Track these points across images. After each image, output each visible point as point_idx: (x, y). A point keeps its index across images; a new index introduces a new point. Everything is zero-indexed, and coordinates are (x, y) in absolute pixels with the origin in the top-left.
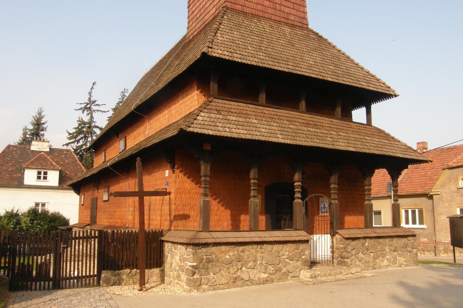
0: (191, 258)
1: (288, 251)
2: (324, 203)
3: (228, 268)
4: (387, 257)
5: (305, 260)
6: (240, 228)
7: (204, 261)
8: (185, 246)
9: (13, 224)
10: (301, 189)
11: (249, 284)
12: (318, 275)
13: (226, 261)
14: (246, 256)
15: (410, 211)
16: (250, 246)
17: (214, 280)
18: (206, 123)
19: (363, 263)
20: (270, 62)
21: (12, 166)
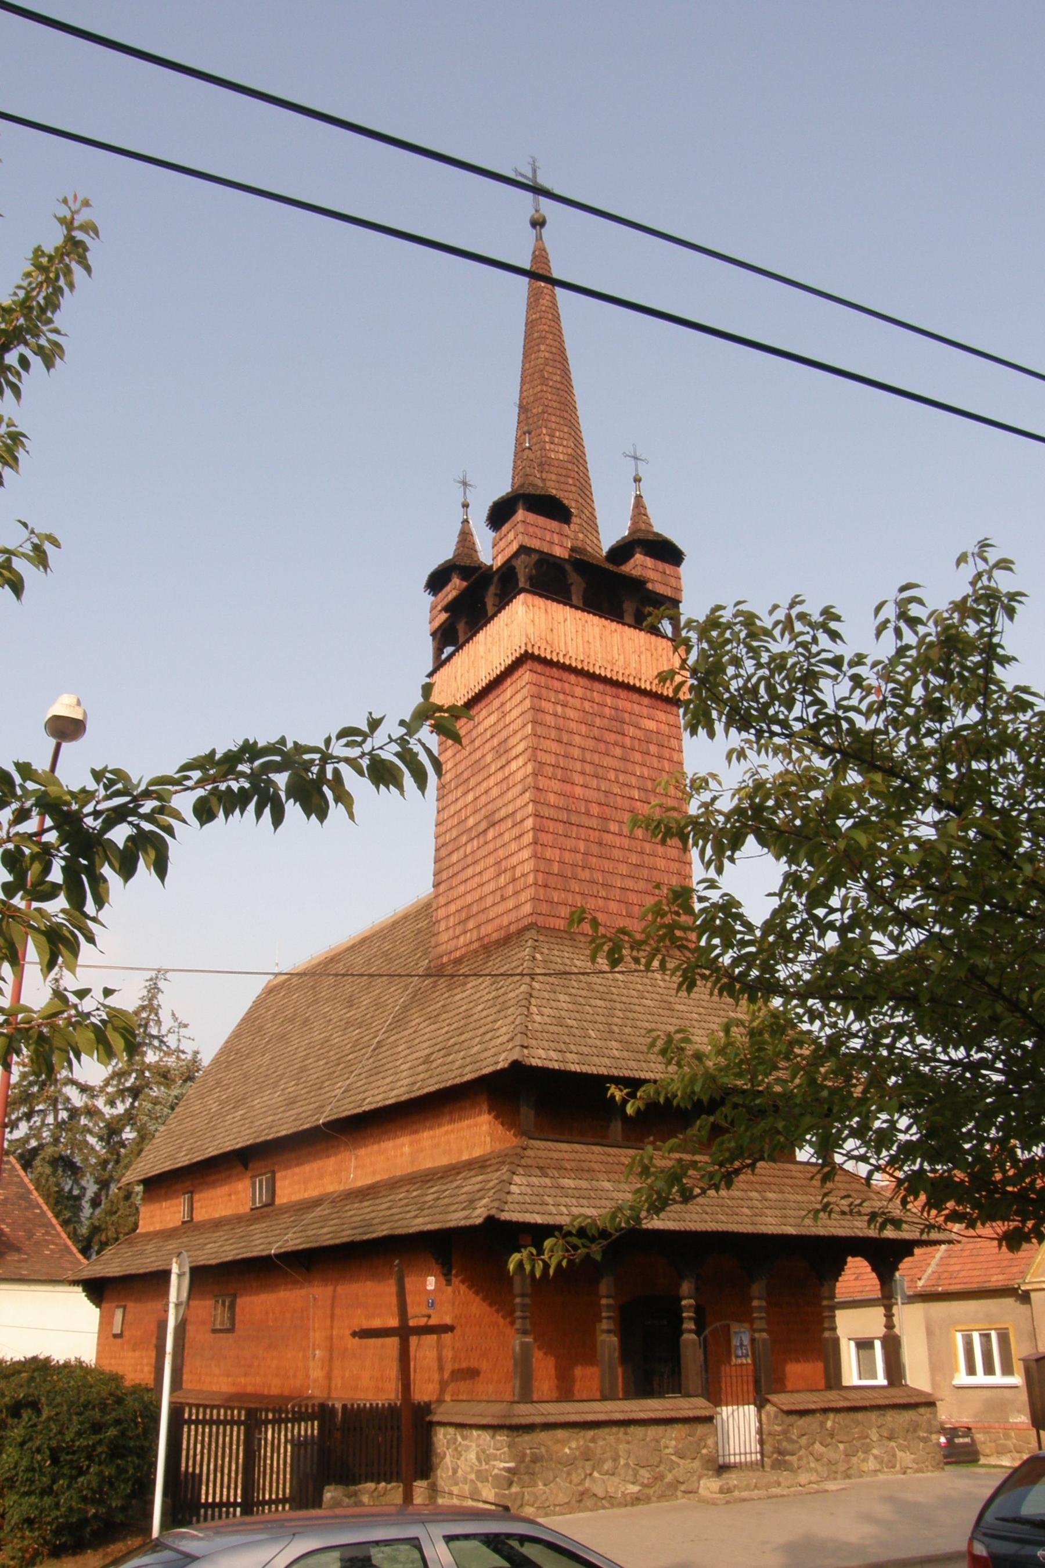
0: (504, 1453)
1: (676, 1439)
2: (741, 1337)
3: (569, 1474)
4: (875, 1451)
6: (573, 1395)
7: (528, 1459)
8: (491, 1432)
11: (607, 1505)
12: (735, 1486)
15: (976, 1337)
16: (607, 1430)
17: (544, 1497)
18: (527, 1199)
20: (633, 1064)
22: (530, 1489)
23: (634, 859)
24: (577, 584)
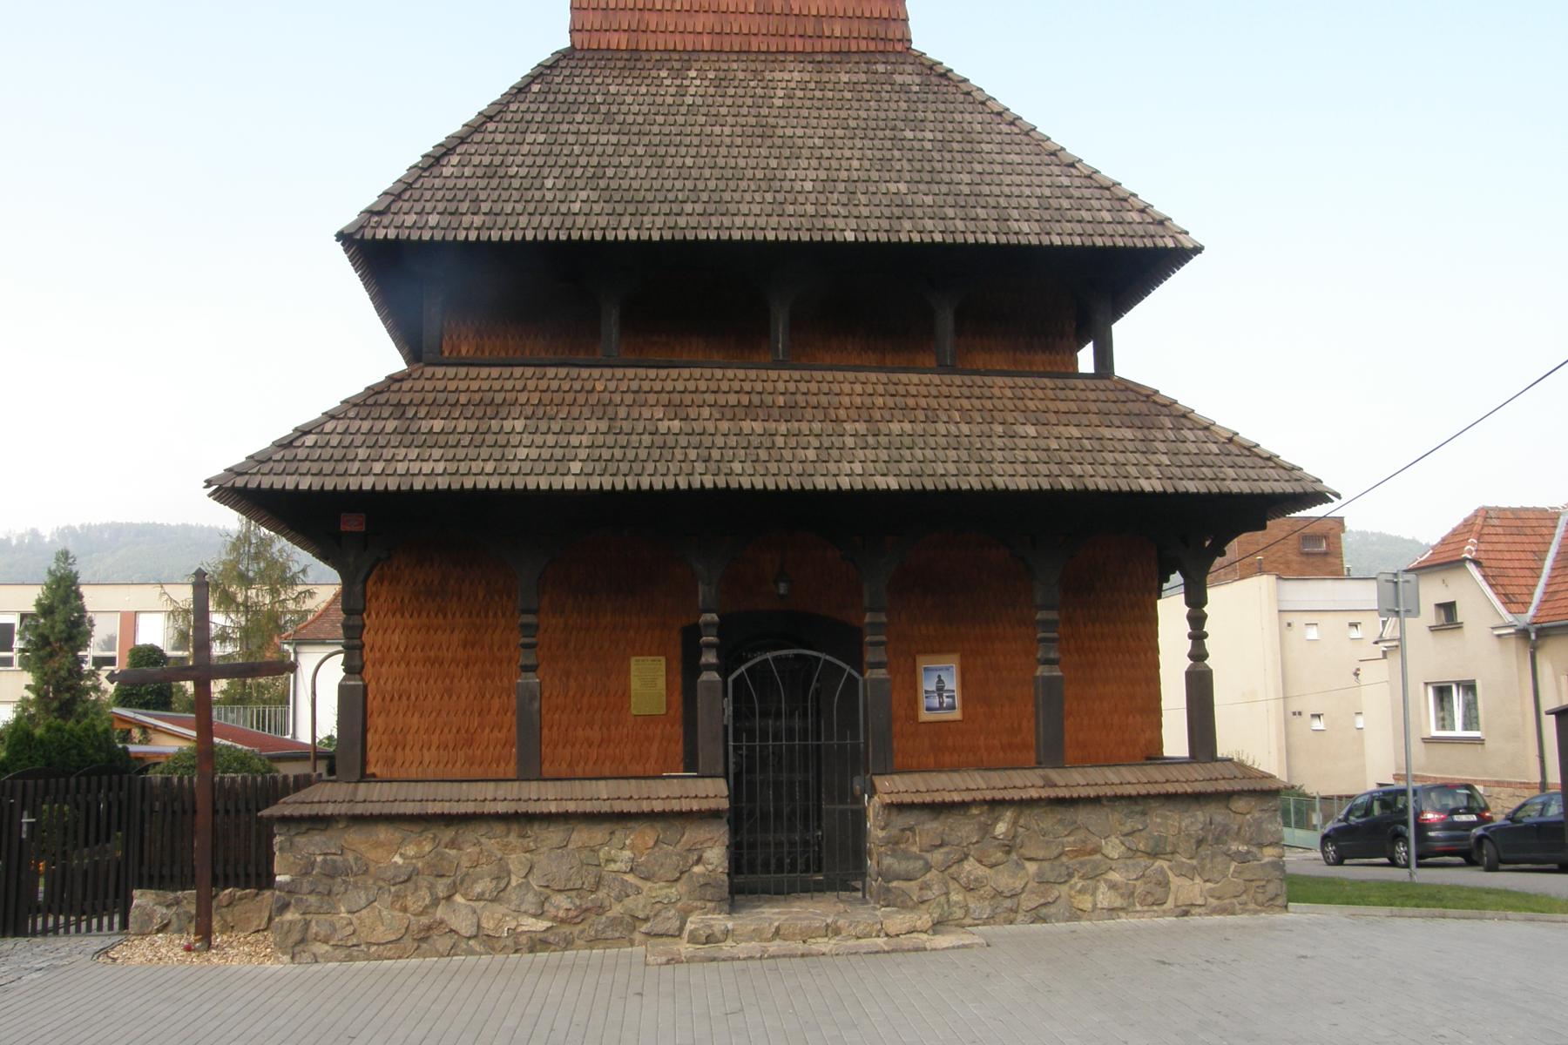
1: (633, 847)
5: (702, 881)
10: (718, 636)
12: (727, 933)
13: (390, 874)
14: (465, 858)
16: (483, 829)
17: (350, 930)
19: (982, 898)
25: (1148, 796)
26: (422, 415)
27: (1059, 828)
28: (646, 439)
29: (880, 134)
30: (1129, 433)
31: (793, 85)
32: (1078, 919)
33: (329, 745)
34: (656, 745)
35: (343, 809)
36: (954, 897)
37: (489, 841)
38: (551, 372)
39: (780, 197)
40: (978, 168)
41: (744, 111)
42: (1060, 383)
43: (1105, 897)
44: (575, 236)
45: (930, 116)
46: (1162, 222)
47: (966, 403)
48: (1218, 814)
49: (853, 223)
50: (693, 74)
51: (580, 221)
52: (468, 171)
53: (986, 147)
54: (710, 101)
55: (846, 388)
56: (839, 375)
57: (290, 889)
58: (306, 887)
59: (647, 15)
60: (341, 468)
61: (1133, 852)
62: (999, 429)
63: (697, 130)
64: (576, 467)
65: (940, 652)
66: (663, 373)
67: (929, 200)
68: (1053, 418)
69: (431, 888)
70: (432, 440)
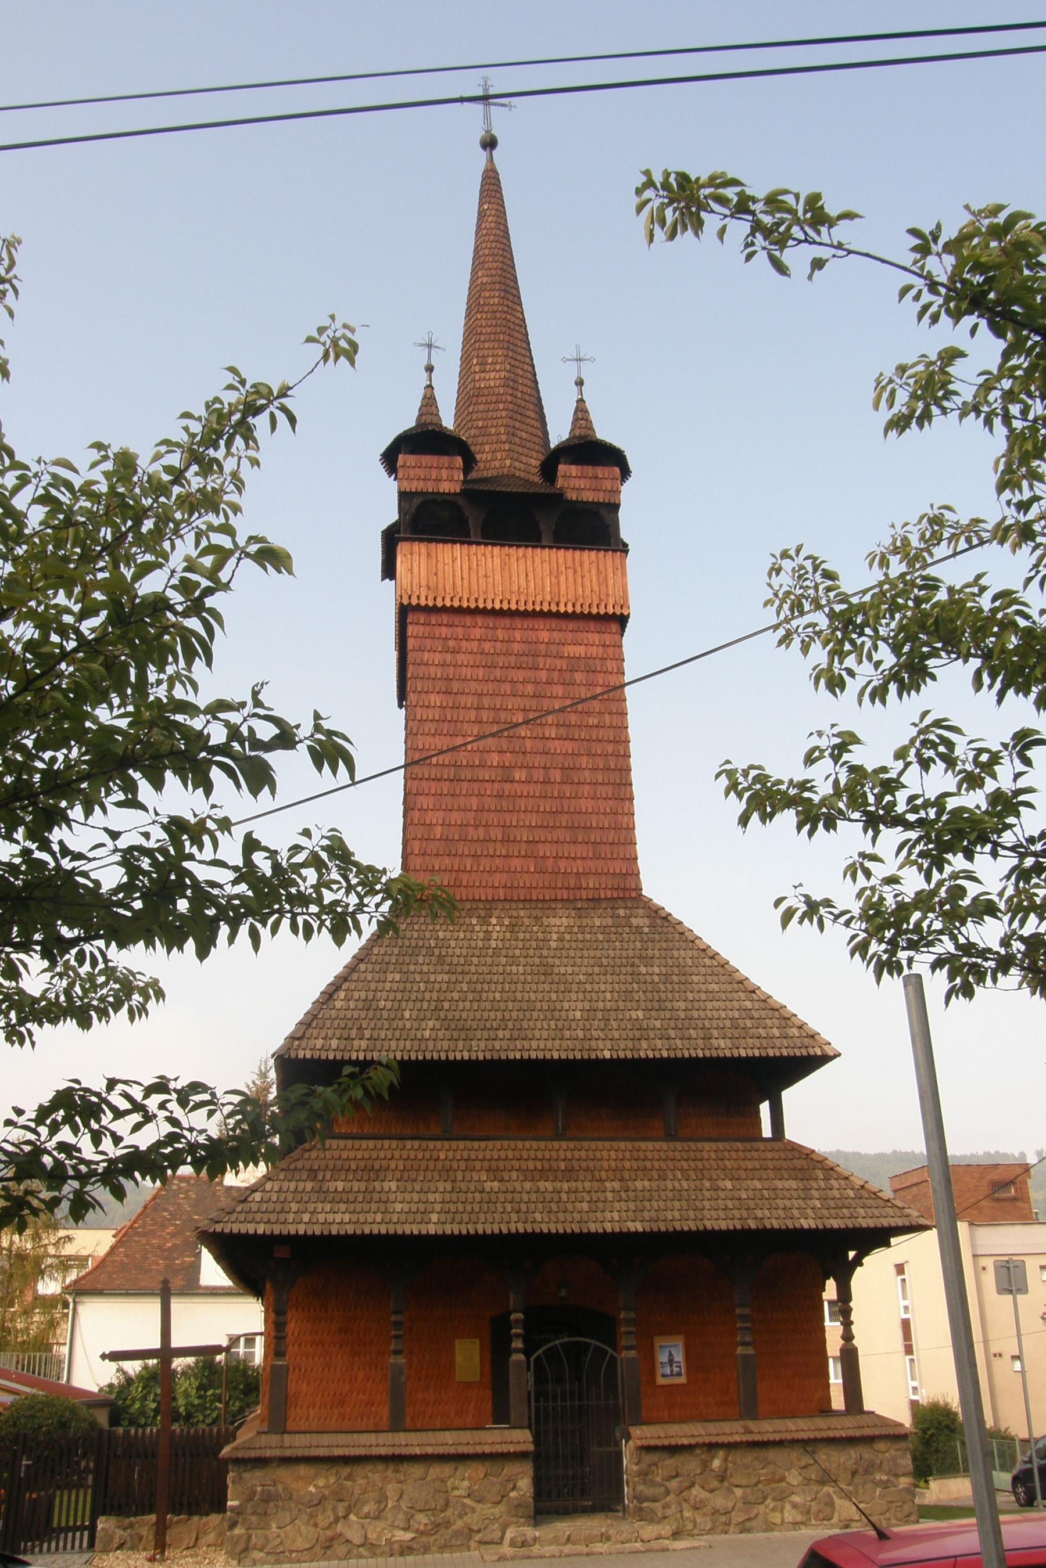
1: (470, 1479)
3: (312, 1516)
9: (154, 1401)
12: (535, 1539)
13: (307, 1498)
16: (370, 1467)
17: (278, 1541)
19: (705, 1515)
21: (173, 1235)
22: (259, 1532)
23: (546, 805)
24: (474, 517)
25: (815, 1440)
26: (328, 1177)
27: (756, 1463)
28: (477, 1195)
29: (623, 970)
30: (793, 1184)
31: (562, 929)
32: (773, 1530)
33: (110, 1392)
34: (473, 1404)
35: (278, 1453)
36: (686, 1514)
37: (374, 1475)
38: (409, 1144)
39: (560, 1024)
40: (690, 996)
41: (531, 952)
42: (748, 1145)
43: (790, 1514)
44: (428, 1057)
45: (657, 953)
46: (813, 1036)
47: (685, 1164)
48: (865, 1453)
49: (608, 1043)
50: (494, 921)
51: (431, 1044)
52: (352, 1004)
53: (695, 978)
54: (507, 944)
55: (605, 1154)
56: (600, 1144)
57: (238, 1511)
58: (249, 1510)
59: (461, 875)
60: (282, 1217)
61: (808, 1481)
62: (707, 1184)
63: (501, 969)
64: (434, 1217)
65: (670, 1333)
66: (483, 1144)
67: (658, 1024)
68: (743, 1174)
69: (334, 1509)
70: (339, 1198)
